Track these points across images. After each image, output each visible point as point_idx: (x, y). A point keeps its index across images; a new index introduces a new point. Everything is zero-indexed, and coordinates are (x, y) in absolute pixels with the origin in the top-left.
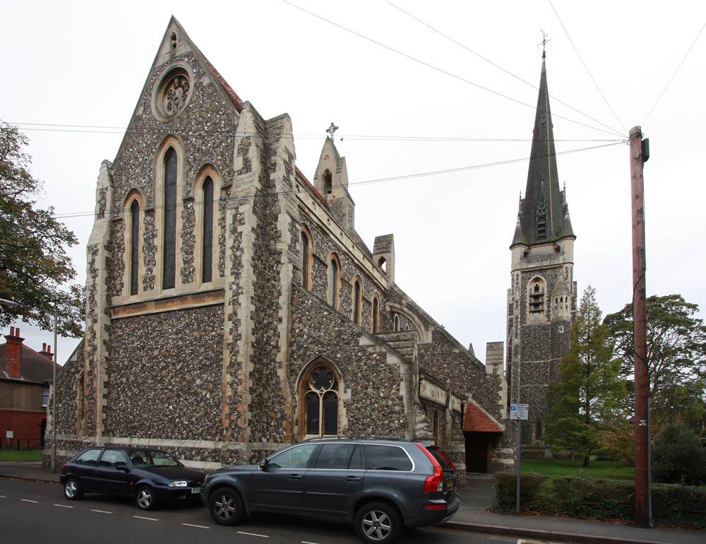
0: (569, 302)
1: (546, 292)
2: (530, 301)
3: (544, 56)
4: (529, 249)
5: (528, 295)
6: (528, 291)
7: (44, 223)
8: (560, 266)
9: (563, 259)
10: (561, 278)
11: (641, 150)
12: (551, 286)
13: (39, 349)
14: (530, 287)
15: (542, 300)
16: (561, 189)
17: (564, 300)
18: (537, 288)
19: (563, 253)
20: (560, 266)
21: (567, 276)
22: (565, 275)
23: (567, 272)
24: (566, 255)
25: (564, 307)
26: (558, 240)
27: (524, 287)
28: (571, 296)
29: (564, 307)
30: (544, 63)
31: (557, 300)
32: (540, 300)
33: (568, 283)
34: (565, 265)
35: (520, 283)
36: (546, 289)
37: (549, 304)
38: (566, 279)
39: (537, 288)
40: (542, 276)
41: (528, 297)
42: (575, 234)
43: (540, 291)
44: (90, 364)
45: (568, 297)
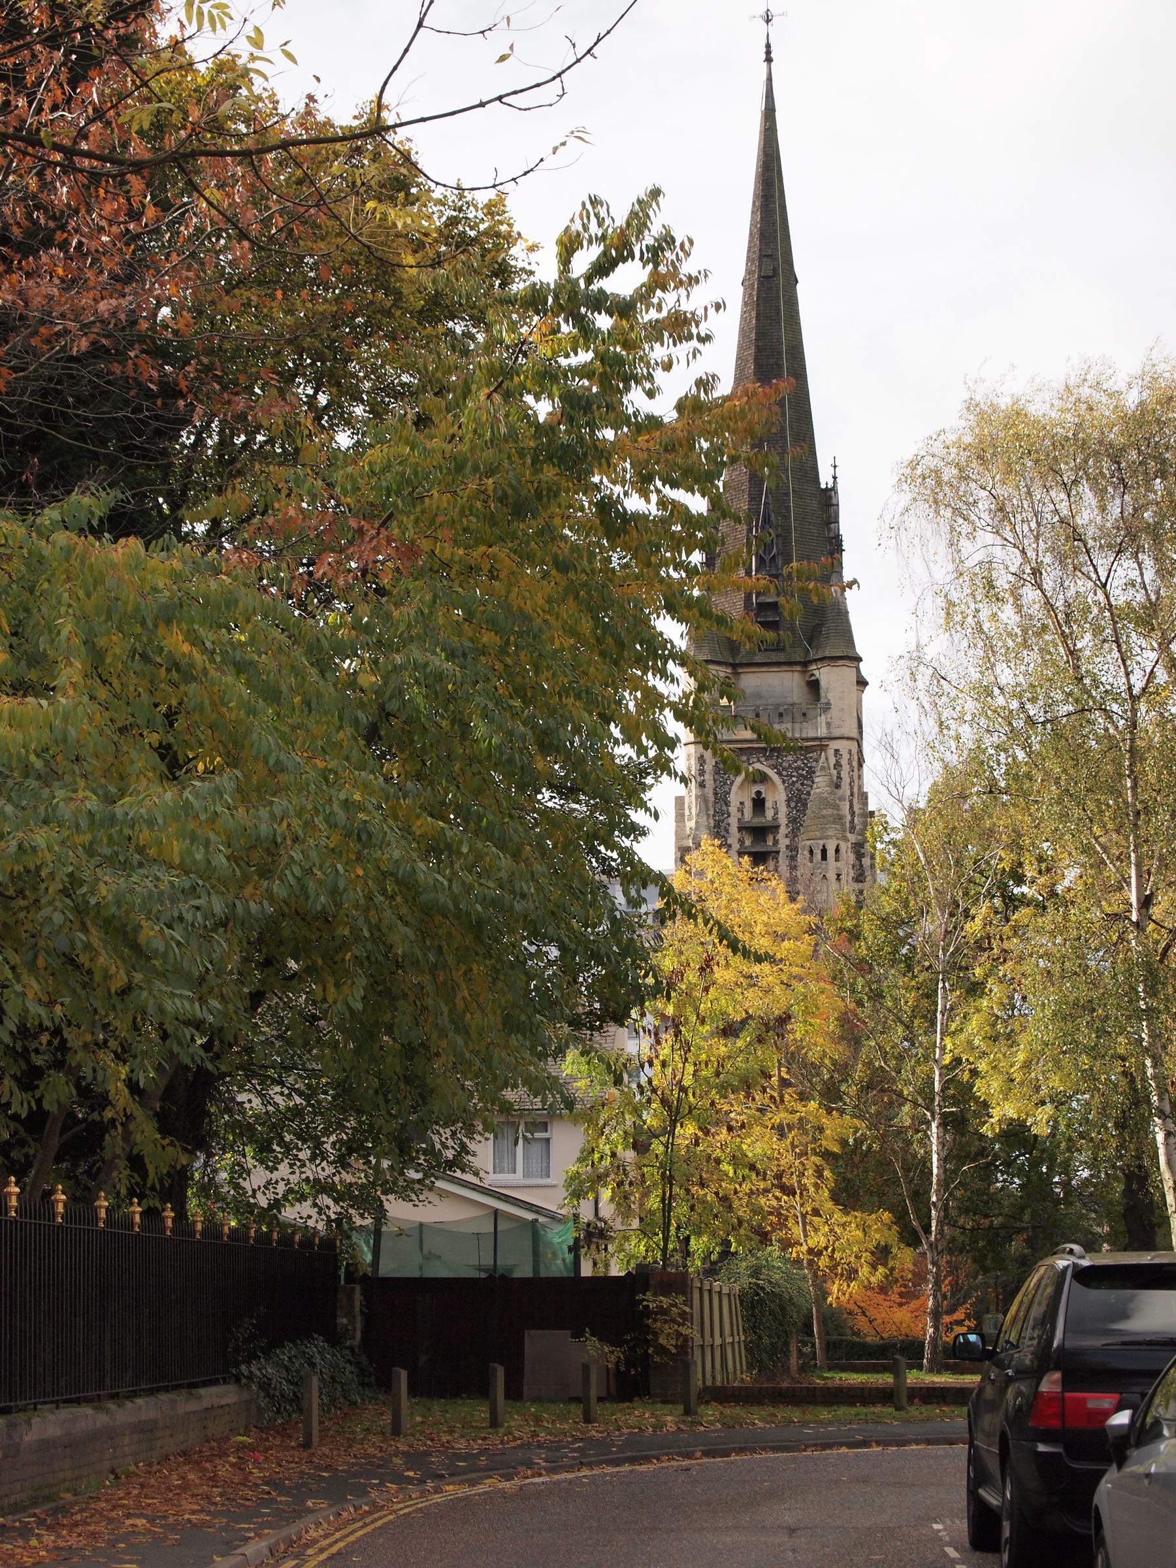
0: (848, 856)
1: (783, 820)
2: (741, 842)
3: (769, 60)
4: (736, 674)
5: (733, 823)
6: (733, 810)
7: (323, 399)
8: (820, 745)
9: (828, 724)
10: (821, 783)
11: (542, 160)
12: (798, 802)
13: (671, 734)
14: (739, 796)
15: (776, 842)
16: (825, 480)
17: (831, 853)
18: (759, 804)
19: (827, 707)
20: (820, 745)
21: (839, 777)
22: (834, 772)
23: (838, 765)
24: (834, 712)
25: (832, 876)
26: (816, 661)
27: (721, 798)
28: (852, 838)
29: (832, 876)
30: (769, 79)
31: (811, 852)
32: (770, 842)
33: (842, 799)
34: (834, 745)
35: (710, 783)
36: (783, 810)
37: (793, 858)
38: (838, 786)
39: (759, 804)
40: (773, 767)
41: (734, 829)
42: (860, 649)
43: (769, 814)
44: (835, 755)
45: (843, 846)
